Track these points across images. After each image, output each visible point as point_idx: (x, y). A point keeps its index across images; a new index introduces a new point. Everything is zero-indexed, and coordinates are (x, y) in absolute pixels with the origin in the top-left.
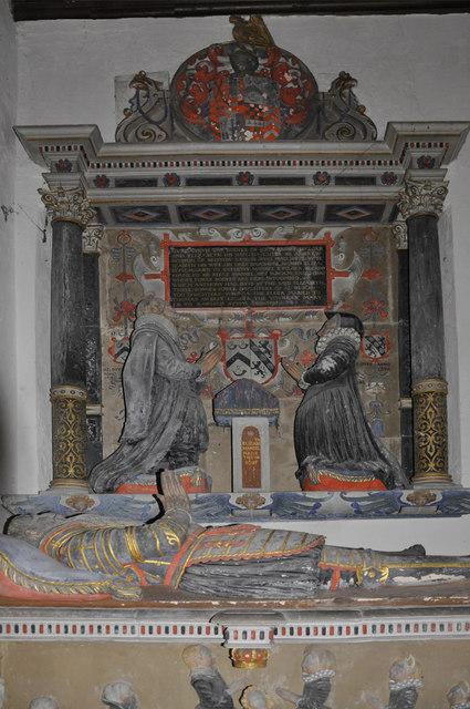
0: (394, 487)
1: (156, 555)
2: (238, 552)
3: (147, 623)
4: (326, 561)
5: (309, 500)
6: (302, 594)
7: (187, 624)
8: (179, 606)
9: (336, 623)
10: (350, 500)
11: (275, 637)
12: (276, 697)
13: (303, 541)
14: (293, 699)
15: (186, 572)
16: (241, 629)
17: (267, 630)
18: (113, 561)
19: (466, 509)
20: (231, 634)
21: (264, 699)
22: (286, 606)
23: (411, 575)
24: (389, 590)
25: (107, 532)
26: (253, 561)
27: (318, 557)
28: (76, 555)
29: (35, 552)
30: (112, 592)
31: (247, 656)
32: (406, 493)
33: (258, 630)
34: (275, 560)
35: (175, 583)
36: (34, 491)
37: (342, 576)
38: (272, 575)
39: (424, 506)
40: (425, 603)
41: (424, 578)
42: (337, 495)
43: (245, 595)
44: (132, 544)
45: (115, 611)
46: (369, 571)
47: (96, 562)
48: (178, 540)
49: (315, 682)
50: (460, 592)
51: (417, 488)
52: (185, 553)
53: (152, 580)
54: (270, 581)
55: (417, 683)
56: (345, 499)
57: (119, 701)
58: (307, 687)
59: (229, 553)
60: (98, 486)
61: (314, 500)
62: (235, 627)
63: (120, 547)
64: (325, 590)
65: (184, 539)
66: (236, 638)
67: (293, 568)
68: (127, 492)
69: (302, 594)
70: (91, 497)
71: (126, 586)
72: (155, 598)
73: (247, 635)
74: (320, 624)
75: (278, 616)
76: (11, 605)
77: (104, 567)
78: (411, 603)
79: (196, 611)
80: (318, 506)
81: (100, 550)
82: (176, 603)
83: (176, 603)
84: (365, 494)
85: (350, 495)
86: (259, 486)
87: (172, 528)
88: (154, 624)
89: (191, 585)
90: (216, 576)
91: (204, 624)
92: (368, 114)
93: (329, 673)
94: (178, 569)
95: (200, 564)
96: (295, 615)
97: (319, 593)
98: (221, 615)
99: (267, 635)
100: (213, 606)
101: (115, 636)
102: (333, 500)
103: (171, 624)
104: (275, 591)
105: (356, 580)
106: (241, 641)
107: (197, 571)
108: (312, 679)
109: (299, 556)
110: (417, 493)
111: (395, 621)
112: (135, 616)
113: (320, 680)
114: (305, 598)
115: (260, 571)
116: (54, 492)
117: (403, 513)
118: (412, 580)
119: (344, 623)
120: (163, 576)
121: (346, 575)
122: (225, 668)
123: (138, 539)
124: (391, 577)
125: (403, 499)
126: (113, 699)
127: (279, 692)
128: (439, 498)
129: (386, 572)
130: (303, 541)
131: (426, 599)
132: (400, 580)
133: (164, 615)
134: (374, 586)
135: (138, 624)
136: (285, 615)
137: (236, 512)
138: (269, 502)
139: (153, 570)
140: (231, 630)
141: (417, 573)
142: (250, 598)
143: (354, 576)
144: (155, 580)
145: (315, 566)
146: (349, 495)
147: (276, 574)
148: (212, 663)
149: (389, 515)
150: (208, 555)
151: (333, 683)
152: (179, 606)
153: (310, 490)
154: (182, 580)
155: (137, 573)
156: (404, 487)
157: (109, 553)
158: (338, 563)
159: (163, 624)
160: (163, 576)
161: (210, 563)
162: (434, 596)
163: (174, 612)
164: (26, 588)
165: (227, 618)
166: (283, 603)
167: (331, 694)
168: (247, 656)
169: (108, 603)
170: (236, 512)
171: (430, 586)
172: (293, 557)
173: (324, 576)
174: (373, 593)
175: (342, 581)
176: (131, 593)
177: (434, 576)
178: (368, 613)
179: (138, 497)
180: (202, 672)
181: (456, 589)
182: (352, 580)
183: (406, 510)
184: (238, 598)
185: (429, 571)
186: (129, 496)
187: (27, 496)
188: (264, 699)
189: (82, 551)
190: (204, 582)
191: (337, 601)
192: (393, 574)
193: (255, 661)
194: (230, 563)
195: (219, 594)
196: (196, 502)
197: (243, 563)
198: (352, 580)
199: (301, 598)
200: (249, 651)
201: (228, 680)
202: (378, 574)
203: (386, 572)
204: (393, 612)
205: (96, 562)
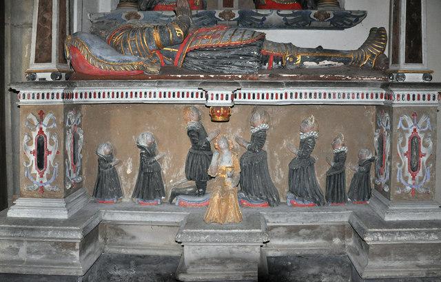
0: (307, 8)
1: (171, 44)
2: (216, 42)
3: (163, 90)
4: (267, 50)
5: (259, 15)
6: (251, 71)
7: (185, 91)
8: (181, 78)
9: (270, 91)
10: (282, 15)
11: (235, 100)
12: (235, 143)
13: (253, 35)
14: (245, 144)
15: (186, 56)
16: (215, 93)
17: (230, 93)
18: (146, 49)
19: (346, 24)
20: (210, 96)
21: (228, 143)
22: (242, 78)
23: (314, 61)
24: (300, 68)
25: (143, 29)
26: (224, 48)
27: (261, 46)
28: (125, 44)
29: (103, 44)
30: (144, 69)
31: (218, 112)
32: (314, 12)
33: (225, 93)
34: (236, 47)
35: (180, 63)
36: (108, 10)
37: (274, 60)
38: (234, 58)
39: (323, 21)
40: (321, 79)
41: (321, 63)
42: (275, 12)
43: (219, 70)
44: (157, 36)
45: (145, 82)
46: (290, 57)
47: (136, 49)
48: (182, 33)
49: (257, 132)
50: (340, 73)
51: (320, 9)
52: (186, 45)
53: (168, 62)
54: (233, 61)
55: (315, 134)
56: (279, 14)
57: (146, 145)
58: (253, 136)
59: (212, 42)
60: (143, 6)
61: (262, 15)
62: (213, 91)
63: (150, 39)
64: (264, 69)
65: (186, 33)
66: (212, 99)
67: (246, 53)
68: (159, 10)
69: (251, 71)
70: (139, 13)
71: (152, 64)
72: (167, 74)
73: (219, 96)
74: (261, 91)
75: (236, 84)
76: (89, 79)
77: (140, 52)
78: (312, 78)
79: (191, 81)
80: (264, 19)
81: (139, 41)
82: (180, 76)
83: (180, 76)
84: (290, 12)
85: (282, 12)
86: (233, 7)
87: (179, 26)
88: (167, 90)
89: (189, 65)
90: (203, 58)
91: (195, 90)
92: (324, 48)
93: (265, 126)
94: (181, 54)
95: (194, 50)
96: (246, 85)
97: (261, 70)
98: (204, 83)
99: (230, 97)
100: (199, 78)
101: (145, 99)
102: (273, 15)
103: (176, 90)
104: (236, 68)
105: (282, 63)
106: (215, 101)
107: (193, 55)
108: (256, 130)
109: (250, 45)
110: (319, 12)
111: (304, 90)
112: (156, 85)
113: (260, 131)
114: (253, 73)
115: (228, 55)
116: (120, 10)
117: (312, 25)
118: (314, 64)
119: (274, 91)
120: (173, 59)
121: (277, 59)
122: (207, 123)
123: (160, 33)
124: (302, 61)
125: (312, 16)
126: (143, 144)
127: (237, 140)
128: (332, 16)
129: (299, 58)
130: (253, 35)
131: (321, 76)
132: (308, 64)
133: (173, 84)
134: (292, 67)
135: (157, 90)
136: (241, 84)
137: (219, 22)
138: (237, 16)
139: (169, 55)
140: (209, 93)
141: (317, 60)
142: (222, 73)
143: (281, 60)
144: (169, 61)
145: (259, 51)
146: (281, 13)
147: (236, 57)
148: (199, 119)
149: (303, 27)
150: (200, 43)
151: (268, 134)
152: (181, 78)
153: (261, 9)
154: (184, 62)
155: (159, 58)
156: (312, 9)
157: (144, 43)
158: (273, 52)
159: (172, 90)
160: (173, 59)
161: (200, 50)
162: (326, 74)
163: (178, 82)
164: (98, 67)
165: (207, 85)
166: (240, 76)
167: (267, 141)
168: (218, 112)
169: (140, 77)
170: (219, 22)
171: (324, 68)
172: (247, 45)
173: (263, 60)
174: (292, 72)
175: (274, 63)
176: (154, 70)
177: (326, 62)
178: (288, 84)
179: (165, 13)
180: (193, 125)
181: (338, 70)
182: (280, 63)
183: (314, 24)
184: (215, 73)
185: (323, 58)
186: (160, 12)
187: (104, 14)
188: (228, 143)
189: (129, 42)
190: (196, 62)
191: (271, 76)
192: (304, 59)
193: (223, 115)
194: (211, 49)
195: (205, 70)
196: (197, 16)
197: (219, 49)
198: (280, 63)
199: (250, 73)
200: (219, 108)
201: (208, 130)
202: (295, 60)
203: (299, 58)
204: (302, 84)
205: (136, 49)
